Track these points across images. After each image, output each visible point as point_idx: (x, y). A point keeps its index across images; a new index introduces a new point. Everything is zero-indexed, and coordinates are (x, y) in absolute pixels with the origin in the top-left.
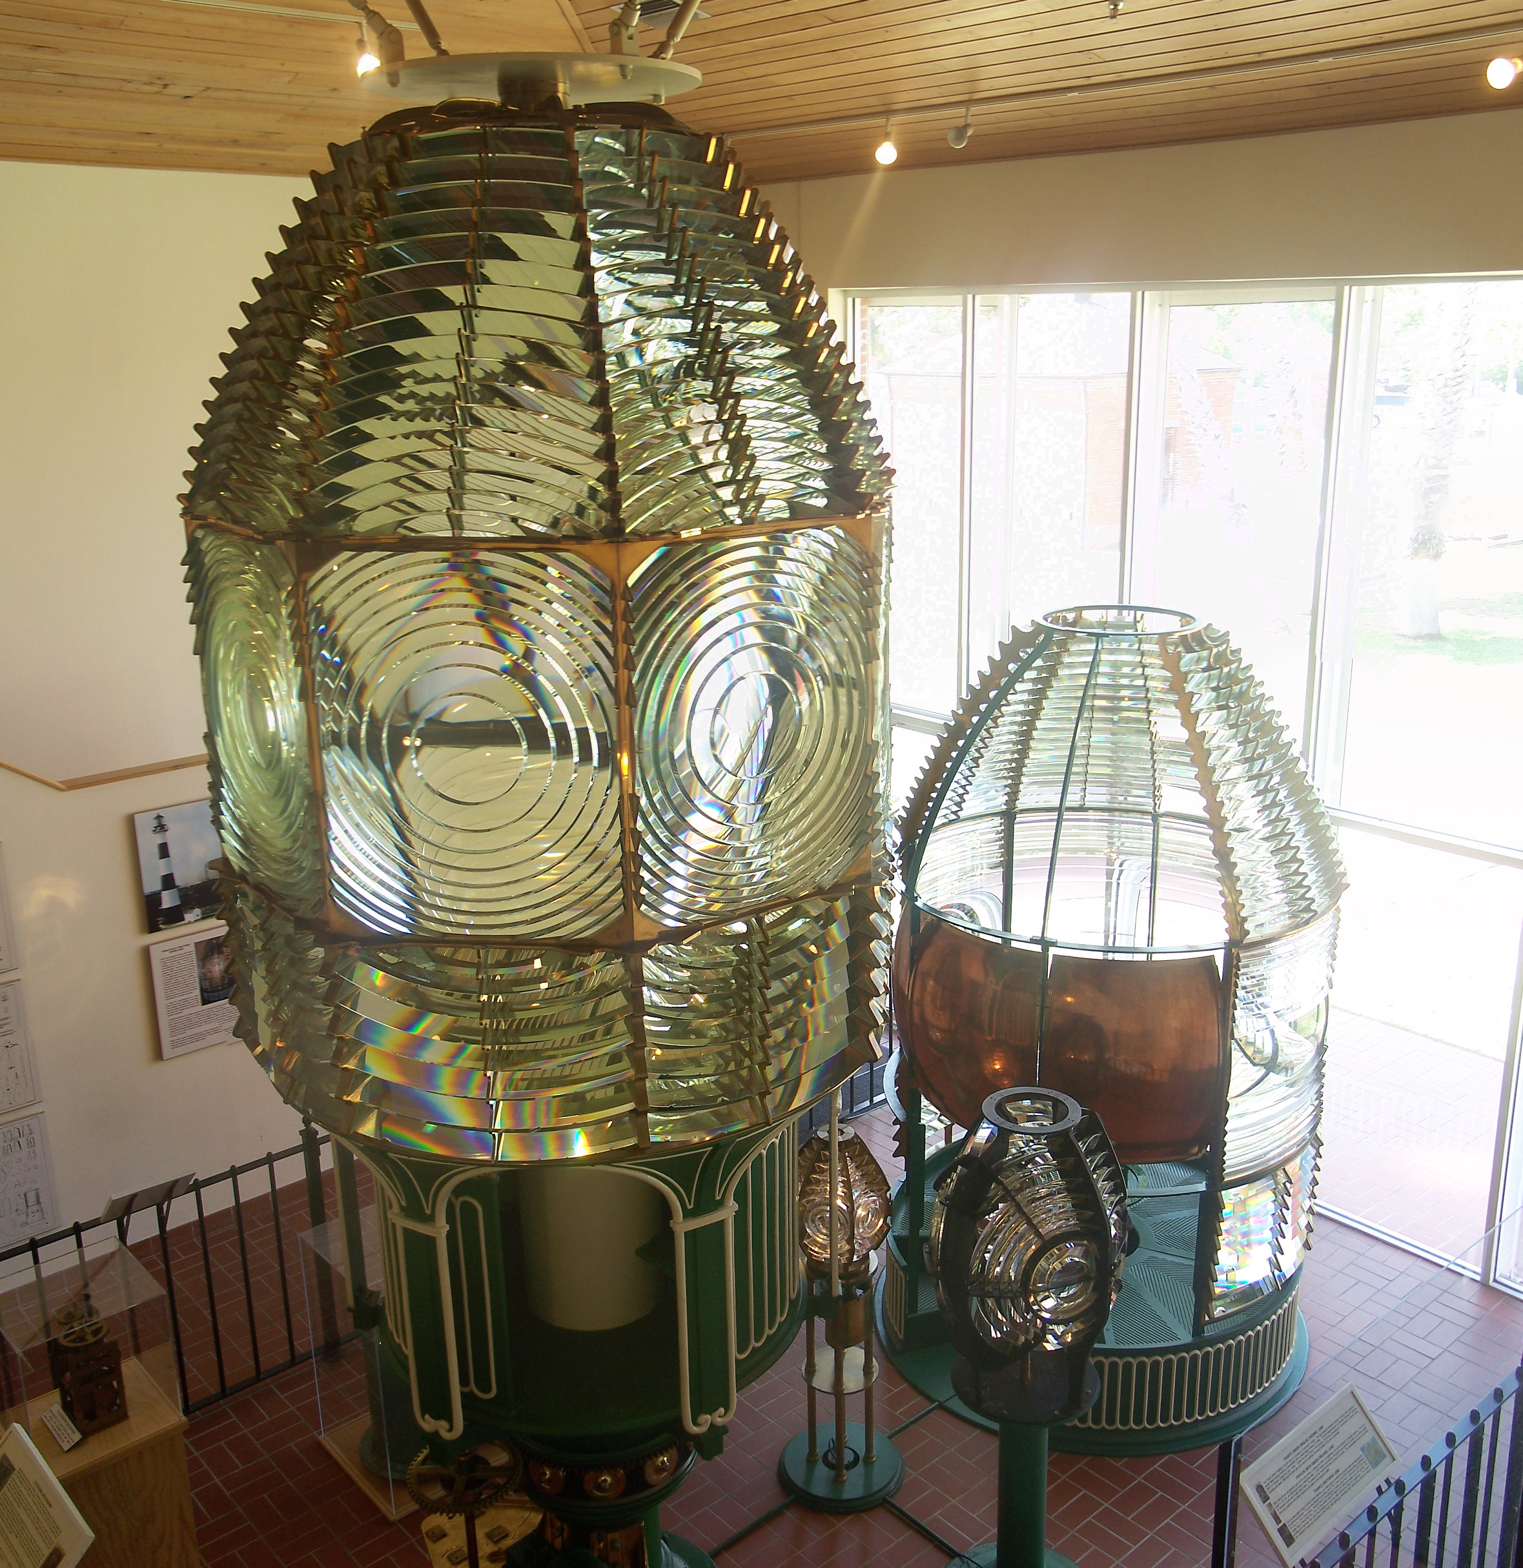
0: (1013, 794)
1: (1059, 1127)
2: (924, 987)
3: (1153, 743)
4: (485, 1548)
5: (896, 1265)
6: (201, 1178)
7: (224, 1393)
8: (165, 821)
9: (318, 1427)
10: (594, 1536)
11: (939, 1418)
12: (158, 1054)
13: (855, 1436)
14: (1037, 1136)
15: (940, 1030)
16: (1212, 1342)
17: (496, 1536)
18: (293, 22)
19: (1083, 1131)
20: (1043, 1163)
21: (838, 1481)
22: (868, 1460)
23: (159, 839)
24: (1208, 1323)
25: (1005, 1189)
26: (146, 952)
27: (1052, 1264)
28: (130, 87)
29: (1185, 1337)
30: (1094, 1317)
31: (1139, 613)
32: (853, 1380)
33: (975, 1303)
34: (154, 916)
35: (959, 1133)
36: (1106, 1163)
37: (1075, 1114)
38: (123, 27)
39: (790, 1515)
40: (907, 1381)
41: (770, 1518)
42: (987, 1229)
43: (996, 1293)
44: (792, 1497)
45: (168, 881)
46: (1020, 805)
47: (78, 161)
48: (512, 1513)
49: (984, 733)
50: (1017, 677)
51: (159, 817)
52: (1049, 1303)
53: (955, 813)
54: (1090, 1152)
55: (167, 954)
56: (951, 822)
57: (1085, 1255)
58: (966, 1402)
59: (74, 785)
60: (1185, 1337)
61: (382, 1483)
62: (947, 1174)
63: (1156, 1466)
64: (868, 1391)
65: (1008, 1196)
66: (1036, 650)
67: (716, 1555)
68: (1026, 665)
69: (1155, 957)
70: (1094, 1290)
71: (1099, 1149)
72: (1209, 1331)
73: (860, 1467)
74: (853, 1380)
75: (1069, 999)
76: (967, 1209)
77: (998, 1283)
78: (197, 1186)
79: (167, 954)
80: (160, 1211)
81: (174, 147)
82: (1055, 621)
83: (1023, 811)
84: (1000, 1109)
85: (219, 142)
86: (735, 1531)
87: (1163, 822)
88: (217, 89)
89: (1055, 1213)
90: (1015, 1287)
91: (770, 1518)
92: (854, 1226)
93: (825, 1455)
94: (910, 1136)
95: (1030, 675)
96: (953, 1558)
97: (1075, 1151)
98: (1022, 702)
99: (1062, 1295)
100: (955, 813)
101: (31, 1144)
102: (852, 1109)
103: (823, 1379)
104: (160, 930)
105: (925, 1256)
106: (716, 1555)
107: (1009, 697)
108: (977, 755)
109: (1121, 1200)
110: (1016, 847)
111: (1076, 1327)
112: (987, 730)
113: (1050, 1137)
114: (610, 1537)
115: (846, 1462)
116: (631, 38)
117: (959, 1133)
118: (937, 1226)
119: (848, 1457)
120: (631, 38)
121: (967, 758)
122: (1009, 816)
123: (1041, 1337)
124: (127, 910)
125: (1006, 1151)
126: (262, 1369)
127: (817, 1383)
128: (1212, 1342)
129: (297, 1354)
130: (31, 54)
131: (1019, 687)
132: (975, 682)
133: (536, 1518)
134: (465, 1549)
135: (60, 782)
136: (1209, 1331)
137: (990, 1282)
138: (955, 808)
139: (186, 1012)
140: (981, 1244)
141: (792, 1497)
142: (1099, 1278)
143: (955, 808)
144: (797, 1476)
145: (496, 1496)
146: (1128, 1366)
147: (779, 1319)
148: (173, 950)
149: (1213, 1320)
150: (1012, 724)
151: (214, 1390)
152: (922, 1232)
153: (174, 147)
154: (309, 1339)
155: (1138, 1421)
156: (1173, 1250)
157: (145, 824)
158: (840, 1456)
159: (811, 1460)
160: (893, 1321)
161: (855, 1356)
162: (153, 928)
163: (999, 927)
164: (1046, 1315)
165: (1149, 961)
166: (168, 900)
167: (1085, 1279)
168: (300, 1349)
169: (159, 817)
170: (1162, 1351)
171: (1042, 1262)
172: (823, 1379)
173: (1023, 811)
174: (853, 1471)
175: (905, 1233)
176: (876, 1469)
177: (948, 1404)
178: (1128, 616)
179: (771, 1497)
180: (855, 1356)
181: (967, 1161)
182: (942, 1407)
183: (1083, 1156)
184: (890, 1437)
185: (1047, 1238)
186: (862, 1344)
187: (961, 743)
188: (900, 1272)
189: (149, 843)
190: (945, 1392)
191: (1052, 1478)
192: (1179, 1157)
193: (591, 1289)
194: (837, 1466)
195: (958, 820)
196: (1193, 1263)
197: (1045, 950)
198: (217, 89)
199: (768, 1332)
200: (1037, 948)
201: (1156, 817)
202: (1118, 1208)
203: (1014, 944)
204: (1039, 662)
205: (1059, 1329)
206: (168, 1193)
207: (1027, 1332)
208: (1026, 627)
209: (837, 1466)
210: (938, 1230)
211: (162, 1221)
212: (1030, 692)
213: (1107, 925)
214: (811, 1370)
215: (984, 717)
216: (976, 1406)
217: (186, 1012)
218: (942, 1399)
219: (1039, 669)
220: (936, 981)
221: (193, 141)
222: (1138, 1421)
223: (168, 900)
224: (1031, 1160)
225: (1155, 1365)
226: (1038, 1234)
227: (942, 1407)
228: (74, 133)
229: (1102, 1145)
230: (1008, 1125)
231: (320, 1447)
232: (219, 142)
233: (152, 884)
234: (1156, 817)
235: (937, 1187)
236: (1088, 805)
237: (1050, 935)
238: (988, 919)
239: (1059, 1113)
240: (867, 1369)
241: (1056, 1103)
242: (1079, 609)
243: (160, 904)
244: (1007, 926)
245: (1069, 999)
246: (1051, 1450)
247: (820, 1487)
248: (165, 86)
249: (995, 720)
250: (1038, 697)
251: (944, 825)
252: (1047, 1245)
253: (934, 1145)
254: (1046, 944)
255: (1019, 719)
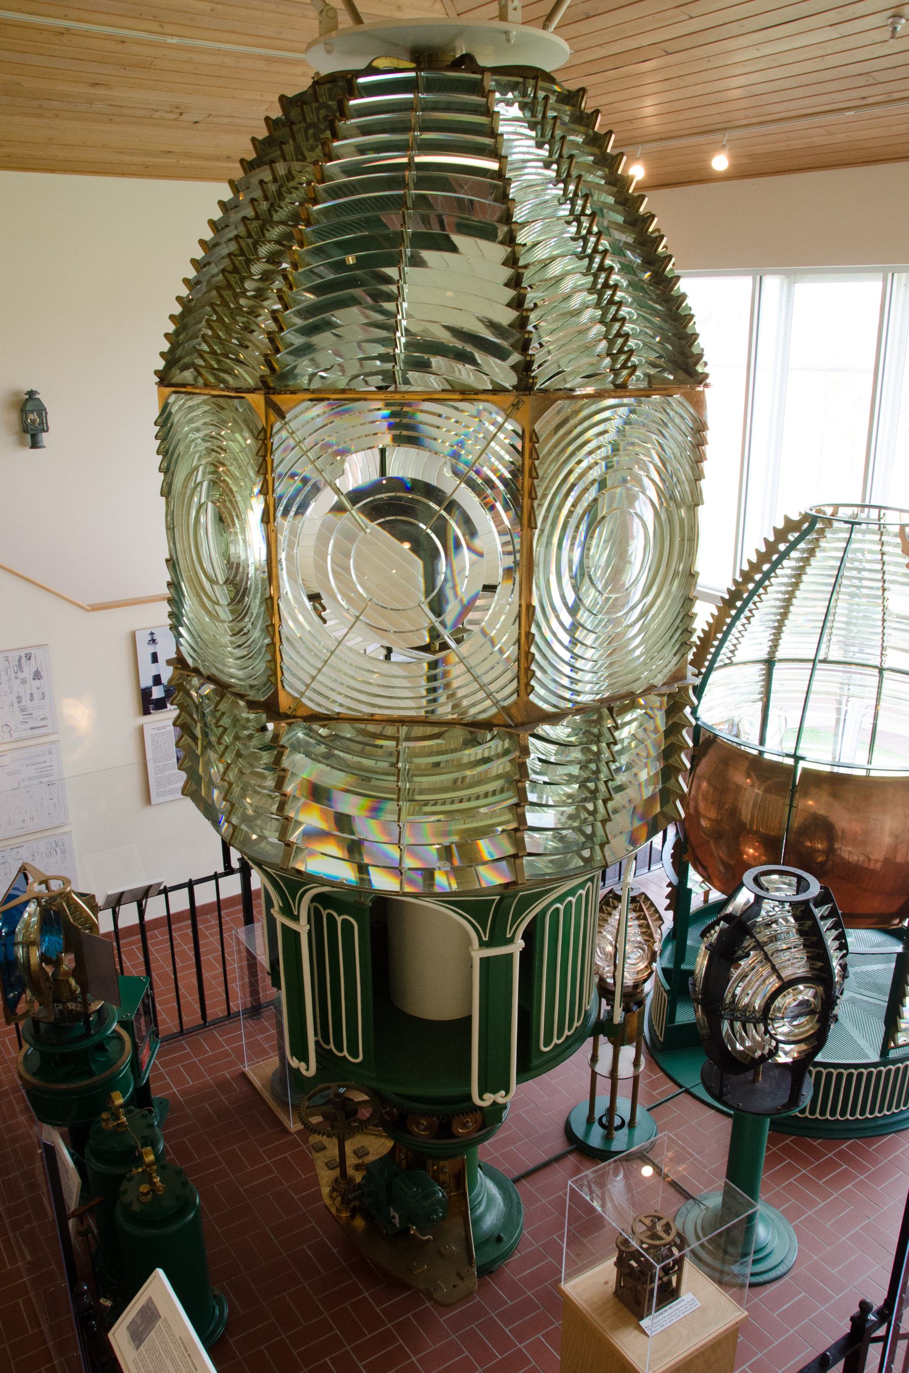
0: (774, 646)
1: (802, 897)
2: (699, 787)
3: (884, 613)
4: (351, 1160)
5: (662, 989)
6: (169, 885)
7: (181, 1032)
8: (155, 637)
9: (243, 1062)
10: (430, 1162)
11: (685, 1099)
12: (148, 800)
13: (623, 1106)
14: (782, 902)
15: (709, 819)
16: (894, 1062)
17: (357, 1153)
18: (270, 60)
19: (820, 901)
20: (787, 924)
21: (608, 1138)
22: (632, 1124)
23: (152, 649)
24: (893, 1048)
25: (757, 941)
26: (141, 730)
27: (788, 1001)
28: (156, 115)
29: (875, 1058)
30: (818, 1040)
31: (883, 511)
32: (625, 1069)
33: (726, 1026)
34: (148, 704)
35: (716, 895)
36: (835, 927)
37: (815, 888)
38: (152, 67)
39: (572, 1159)
40: (663, 1071)
41: (558, 1159)
42: (739, 971)
43: (743, 1019)
44: (574, 1146)
45: (157, 680)
46: (779, 655)
47: (123, 174)
48: (372, 1139)
49: (756, 598)
50: (784, 555)
51: (152, 634)
52: (785, 1029)
53: (729, 658)
54: (823, 918)
55: (155, 731)
56: (726, 665)
57: (815, 996)
58: (708, 1089)
59: (96, 608)
60: (875, 1058)
61: (284, 1105)
62: (712, 926)
63: (843, 1147)
64: (636, 1079)
65: (759, 946)
66: (805, 530)
67: (516, 1181)
68: (793, 546)
69: (873, 774)
70: (818, 1021)
71: (830, 916)
72: (893, 1054)
73: (625, 1130)
74: (625, 1069)
75: (810, 803)
76: (726, 954)
77: (745, 1010)
78: (165, 891)
79: (155, 731)
80: (140, 905)
81: (187, 162)
82: (818, 511)
83: (781, 660)
84: (756, 880)
85: (217, 158)
86: (531, 1166)
87: (886, 674)
88: (217, 116)
89: (794, 963)
90: (758, 1015)
91: (558, 1159)
92: (627, 954)
93: (601, 1118)
94: (679, 895)
95: (794, 554)
96: (687, 1199)
97: (812, 916)
98: (787, 576)
99: (795, 1023)
100: (729, 658)
101: (64, 852)
102: (649, 869)
103: (604, 1066)
104: (150, 713)
105: (690, 986)
106: (516, 1181)
107: (772, 580)
108: (749, 614)
109: (844, 956)
110: (773, 688)
111: (803, 1047)
112: (754, 603)
113: (792, 904)
114: (441, 1163)
115: (615, 1125)
116: (515, 9)
117: (716, 895)
118: (700, 963)
119: (617, 1121)
120: (515, 9)
121: (742, 616)
122: (769, 663)
123: (773, 1053)
124: (131, 701)
125: (758, 915)
126: (185, 1028)
127: (599, 1068)
128: (894, 1062)
129: (232, 1012)
130: (92, 91)
131: (785, 563)
132: (746, 567)
133: (390, 1144)
134: (338, 1160)
135: (89, 606)
136: (893, 1054)
137: (739, 1010)
138: (730, 655)
139: (167, 773)
140: (733, 983)
141: (574, 1146)
142: (823, 1013)
143: (730, 655)
144: (579, 1130)
145: (363, 1127)
146: (829, 1075)
147: (576, 1024)
148: (158, 729)
149: (897, 1047)
150: (777, 592)
151: (176, 1030)
152: (684, 967)
153: (187, 162)
154: (239, 1003)
155: (833, 1114)
156: (864, 992)
157: (142, 640)
158: (611, 1120)
159: (590, 1120)
160: (656, 1028)
161: (628, 1052)
162: (146, 712)
163: (757, 742)
164: (780, 1037)
165: (868, 777)
166: (157, 693)
167: (812, 1012)
168: (234, 1008)
169: (152, 634)
170: (856, 1066)
171: (779, 999)
172: (604, 1066)
173: (781, 660)
174: (620, 1132)
175: (671, 966)
176: (638, 1132)
177: (692, 1090)
178: (874, 513)
179: (558, 1144)
180: (628, 1052)
181: (729, 918)
182: (687, 1091)
183: (818, 920)
184: (648, 1110)
185: (785, 980)
186: (635, 1044)
187: (739, 604)
188: (665, 994)
189: (144, 652)
190: (693, 1080)
191: (768, 1149)
192: (881, 926)
193: (446, 973)
194: (609, 1129)
195: (731, 664)
196: (886, 1004)
197: (796, 762)
198: (217, 116)
199: (567, 1033)
200: (790, 761)
201: (881, 670)
202: (841, 961)
203: (767, 756)
204: (802, 545)
205: (788, 1048)
206: (142, 896)
207: (763, 1049)
208: (795, 517)
209: (609, 1129)
210: (701, 969)
211: (141, 913)
212: (792, 568)
213: (835, 750)
214: (594, 1059)
215: (759, 584)
216: (718, 1098)
217: (167, 773)
218: (688, 1087)
219: (803, 551)
220: (709, 783)
221: (200, 158)
222: (833, 1114)
223: (157, 693)
224: (776, 922)
225: (850, 1076)
226: (779, 977)
227: (687, 1091)
228: (120, 152)
229: (832, 913)
230: (762, 893)
231: (244, 1075)
232: (217, 158)
233: (146, 682)
234: (881, 670)
235: (703, 935)
236: (830, 658)
237: (800, 753)
238: (749, 738)
239: (802, 885)
240: (636, 1063)
241: (800, 879)
242: (837, 506)
243: (151, 695)
244: (762, 741)
245: (810, 803)
246: (770, 1130)
247: (596, 1139)
248: (181, 114)
249: (765, 588)
250: (799, 573)
251: (721, 667)
252: (787, 985)
253: (696, 902)
254: (797, 758)
255: (783, 589)
